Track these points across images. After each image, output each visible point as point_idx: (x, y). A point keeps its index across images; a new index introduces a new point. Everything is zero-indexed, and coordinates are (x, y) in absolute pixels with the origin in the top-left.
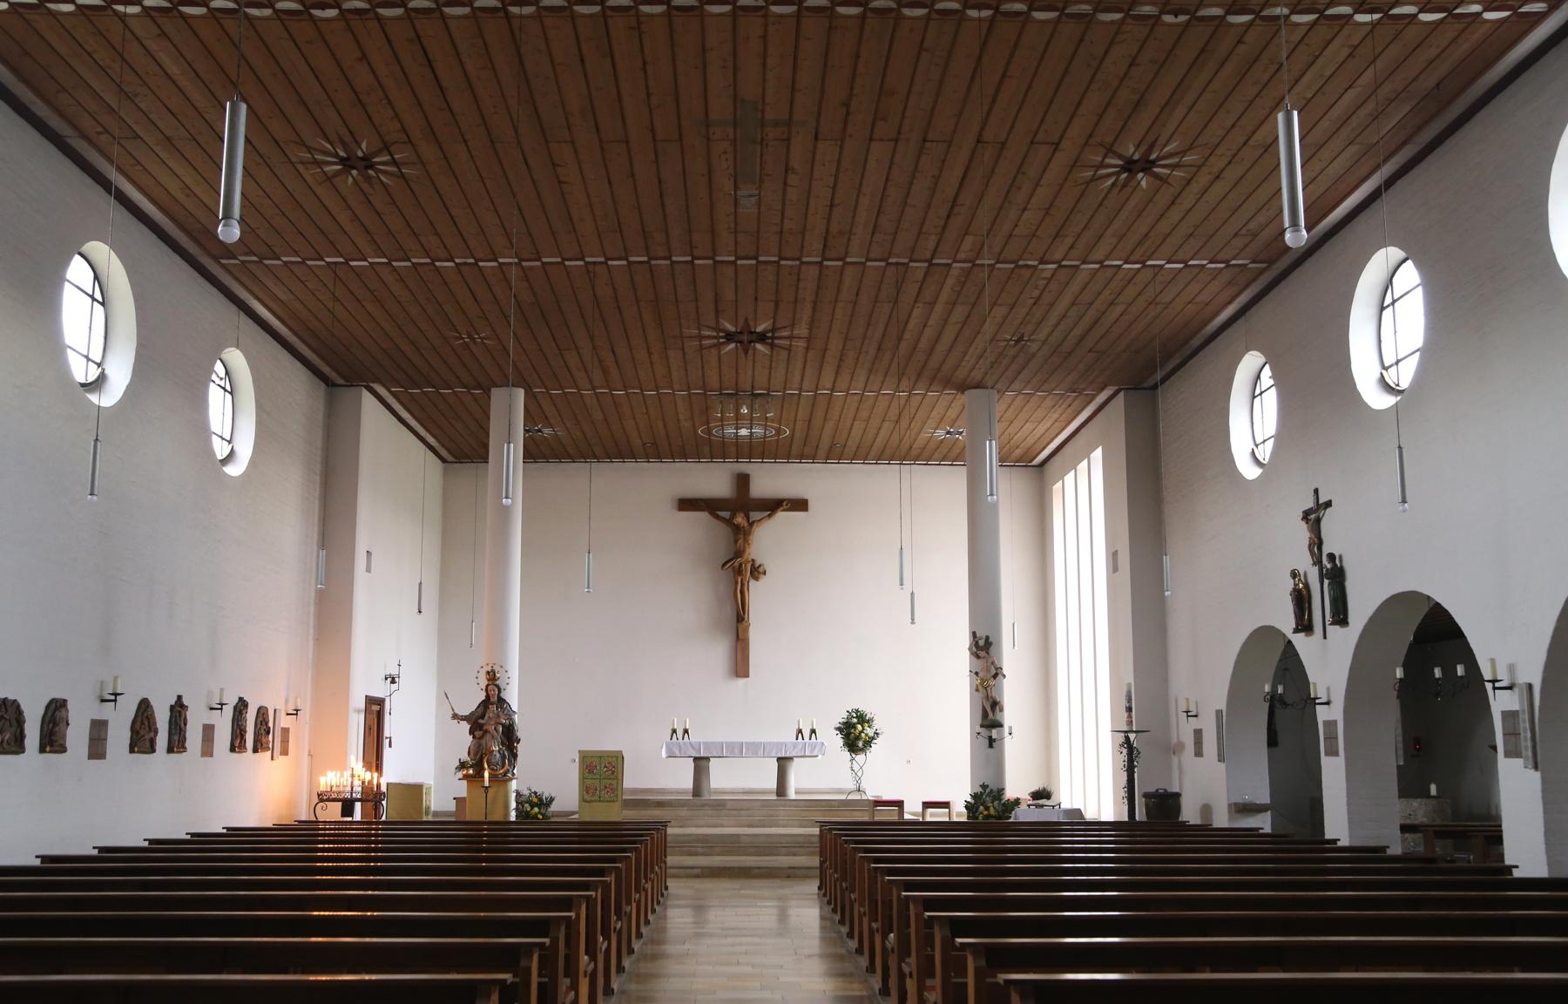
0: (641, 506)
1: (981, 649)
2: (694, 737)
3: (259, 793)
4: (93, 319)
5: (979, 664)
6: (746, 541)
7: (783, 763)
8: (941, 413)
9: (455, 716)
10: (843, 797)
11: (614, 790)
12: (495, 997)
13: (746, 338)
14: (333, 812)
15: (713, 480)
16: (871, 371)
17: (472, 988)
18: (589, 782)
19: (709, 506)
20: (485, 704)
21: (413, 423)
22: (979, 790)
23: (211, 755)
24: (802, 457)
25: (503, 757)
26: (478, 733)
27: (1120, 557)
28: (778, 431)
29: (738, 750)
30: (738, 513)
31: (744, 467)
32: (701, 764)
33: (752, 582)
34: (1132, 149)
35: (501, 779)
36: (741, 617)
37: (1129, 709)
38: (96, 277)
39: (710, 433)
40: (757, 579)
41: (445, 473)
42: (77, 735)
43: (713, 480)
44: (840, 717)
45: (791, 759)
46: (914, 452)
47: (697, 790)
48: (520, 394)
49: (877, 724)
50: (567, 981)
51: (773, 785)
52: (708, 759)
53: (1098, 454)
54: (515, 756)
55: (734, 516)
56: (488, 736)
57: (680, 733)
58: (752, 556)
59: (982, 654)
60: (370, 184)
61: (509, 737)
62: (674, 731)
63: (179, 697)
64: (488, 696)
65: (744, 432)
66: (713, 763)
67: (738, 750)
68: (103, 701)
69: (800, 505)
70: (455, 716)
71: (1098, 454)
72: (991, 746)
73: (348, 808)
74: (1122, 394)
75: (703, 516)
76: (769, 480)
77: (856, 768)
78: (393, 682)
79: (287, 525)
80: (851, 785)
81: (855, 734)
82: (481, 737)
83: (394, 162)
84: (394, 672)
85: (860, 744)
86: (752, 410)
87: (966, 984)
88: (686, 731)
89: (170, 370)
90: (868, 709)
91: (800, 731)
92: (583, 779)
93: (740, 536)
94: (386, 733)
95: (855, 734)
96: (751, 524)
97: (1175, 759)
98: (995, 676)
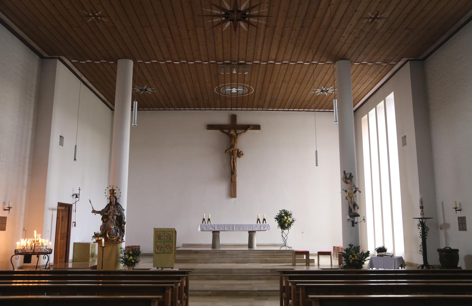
0: (192, 129)
1: (349, 179)
2: (213, 222)
5: (347, 187)
6: (235, 141)
7: (251, 234)
8: (323, 77)
9: (94, 211)
10: (278, 248)
11: (171, 248)
12: (157, 303)
13: (236, 16)
14: (19, 261)
15: (222, 117)
16: (295, 45)
17: (149, 300)
18: (158, 244)
20: (108, 206)
21: (79, 74)
22: (349, 247)
24: (258, 107)
25: (117, 231)
26: (105, 220)
27: (408, 139)
28: (249, 90)
29: (231, 228)
30: (230, 135)
32: (216, 234)
33: (238, 159)
34: (370, 15)
35: (119, 241)
36: (233, 172)
37: (422, 207)
39: (219, 91)
40: (239, 157)
43: (222, 117)
44: (277, 213)
45: (255, 232)
46: (305, 104)
47: (214, 245)
48: (131, 63)
49: (293, 216)
50: (179, 301)
51: (247, 242)
52: (219, 232)
53: (391, 97)
54: (123, 231)
56: (109, 221)
57: (206, 220)
58: (237, 148)
59: (349, 181)
60: (99, 22)
61: (120, 221)
62: (204, 220)
64: (111, 202)
65: (234, 90)
66: (221, 233)
67: (231, 228)
68: (5, 210)
69: (257, 127)
70: (94, 211)
71: (391, 97)
72: (353, 226)
74: (408, 63)
75: (218, 132)
76: (244, 117)
77: (284, 235)
78: (77, 197)
80: (282, 242)
81: (284, 221)
82: (106, 222)
83: (152, 90)
84: (77, 193)
85: (286, 225)
86: (237, 72)
87: (299, 293)
88: (209, 220)
90: (288, 209)
91: (259, 220)
92: (155, 242)
93: (232, 139)
94: (73, 220)
95: (284, 221)
96: (237, 135)
97: (442, 232)
98: (355, 192)
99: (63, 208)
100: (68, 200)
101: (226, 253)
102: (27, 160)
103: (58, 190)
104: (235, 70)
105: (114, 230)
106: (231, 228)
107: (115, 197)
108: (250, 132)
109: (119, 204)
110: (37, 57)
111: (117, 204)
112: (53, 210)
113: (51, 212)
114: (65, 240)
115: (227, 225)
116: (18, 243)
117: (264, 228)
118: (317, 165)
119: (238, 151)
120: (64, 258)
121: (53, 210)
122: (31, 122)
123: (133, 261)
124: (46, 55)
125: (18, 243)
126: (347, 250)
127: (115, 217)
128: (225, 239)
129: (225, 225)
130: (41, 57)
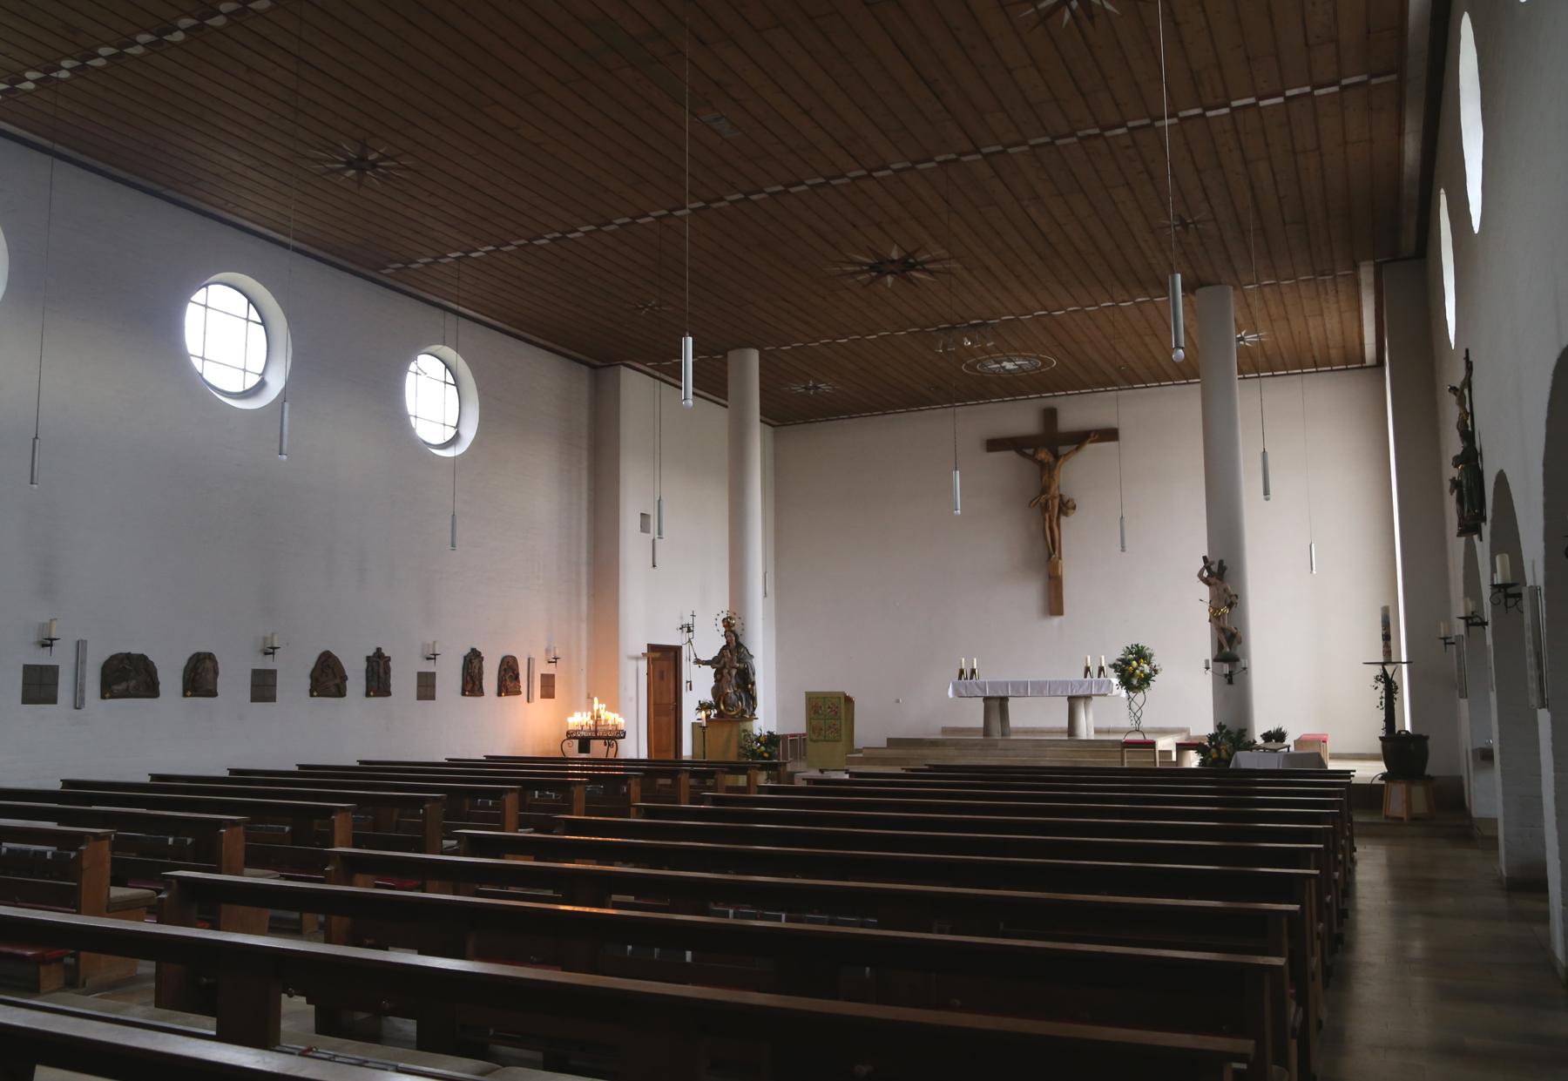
2: (984, 677)
3: (526, 727)
4: (228, 336)
6: (1051, 477)
10: (1121, 737)
14: (573, 750)
15: (1020, 418)
18: (814, 722)
29: (1042, 689)
30: (1047, 448)
31: (1049, 401)
38: (250, 301)
40: (1066, 514)
42: (403, 679)
43: (1020, 418)
44: (1117, 654)
48: (754, 355)
51: (1065, 724)
61: (745, 681)
63: (379, 650)
66: (1013, 705)
69: (1110, 435)
73: (584, 744)
75: (1010, 455)
76: (1077, 412)
79: (540, 497)
85: (1135, 682)
87: (54, 670)
89: (340, 369)
91: (1087, 669)
93: (1047, 471)
96: (1057, 457)
99: (657, 655)
100: (671, 638)
102: (584, 569)
103: (645, 618)
106: (1022, 691)
111: (739, 645)
112: (637, 658)
113: (634, 662)
114: (672, 718)
115: (1014, 684)
116: (570, 720)
118: (1123, 550)
121: (637, 658)
122: (585, 496)
125: (570, 720)
126: (1212, 738)
127: (734, 672)
129: (1007, 684)
130: (593, 367)
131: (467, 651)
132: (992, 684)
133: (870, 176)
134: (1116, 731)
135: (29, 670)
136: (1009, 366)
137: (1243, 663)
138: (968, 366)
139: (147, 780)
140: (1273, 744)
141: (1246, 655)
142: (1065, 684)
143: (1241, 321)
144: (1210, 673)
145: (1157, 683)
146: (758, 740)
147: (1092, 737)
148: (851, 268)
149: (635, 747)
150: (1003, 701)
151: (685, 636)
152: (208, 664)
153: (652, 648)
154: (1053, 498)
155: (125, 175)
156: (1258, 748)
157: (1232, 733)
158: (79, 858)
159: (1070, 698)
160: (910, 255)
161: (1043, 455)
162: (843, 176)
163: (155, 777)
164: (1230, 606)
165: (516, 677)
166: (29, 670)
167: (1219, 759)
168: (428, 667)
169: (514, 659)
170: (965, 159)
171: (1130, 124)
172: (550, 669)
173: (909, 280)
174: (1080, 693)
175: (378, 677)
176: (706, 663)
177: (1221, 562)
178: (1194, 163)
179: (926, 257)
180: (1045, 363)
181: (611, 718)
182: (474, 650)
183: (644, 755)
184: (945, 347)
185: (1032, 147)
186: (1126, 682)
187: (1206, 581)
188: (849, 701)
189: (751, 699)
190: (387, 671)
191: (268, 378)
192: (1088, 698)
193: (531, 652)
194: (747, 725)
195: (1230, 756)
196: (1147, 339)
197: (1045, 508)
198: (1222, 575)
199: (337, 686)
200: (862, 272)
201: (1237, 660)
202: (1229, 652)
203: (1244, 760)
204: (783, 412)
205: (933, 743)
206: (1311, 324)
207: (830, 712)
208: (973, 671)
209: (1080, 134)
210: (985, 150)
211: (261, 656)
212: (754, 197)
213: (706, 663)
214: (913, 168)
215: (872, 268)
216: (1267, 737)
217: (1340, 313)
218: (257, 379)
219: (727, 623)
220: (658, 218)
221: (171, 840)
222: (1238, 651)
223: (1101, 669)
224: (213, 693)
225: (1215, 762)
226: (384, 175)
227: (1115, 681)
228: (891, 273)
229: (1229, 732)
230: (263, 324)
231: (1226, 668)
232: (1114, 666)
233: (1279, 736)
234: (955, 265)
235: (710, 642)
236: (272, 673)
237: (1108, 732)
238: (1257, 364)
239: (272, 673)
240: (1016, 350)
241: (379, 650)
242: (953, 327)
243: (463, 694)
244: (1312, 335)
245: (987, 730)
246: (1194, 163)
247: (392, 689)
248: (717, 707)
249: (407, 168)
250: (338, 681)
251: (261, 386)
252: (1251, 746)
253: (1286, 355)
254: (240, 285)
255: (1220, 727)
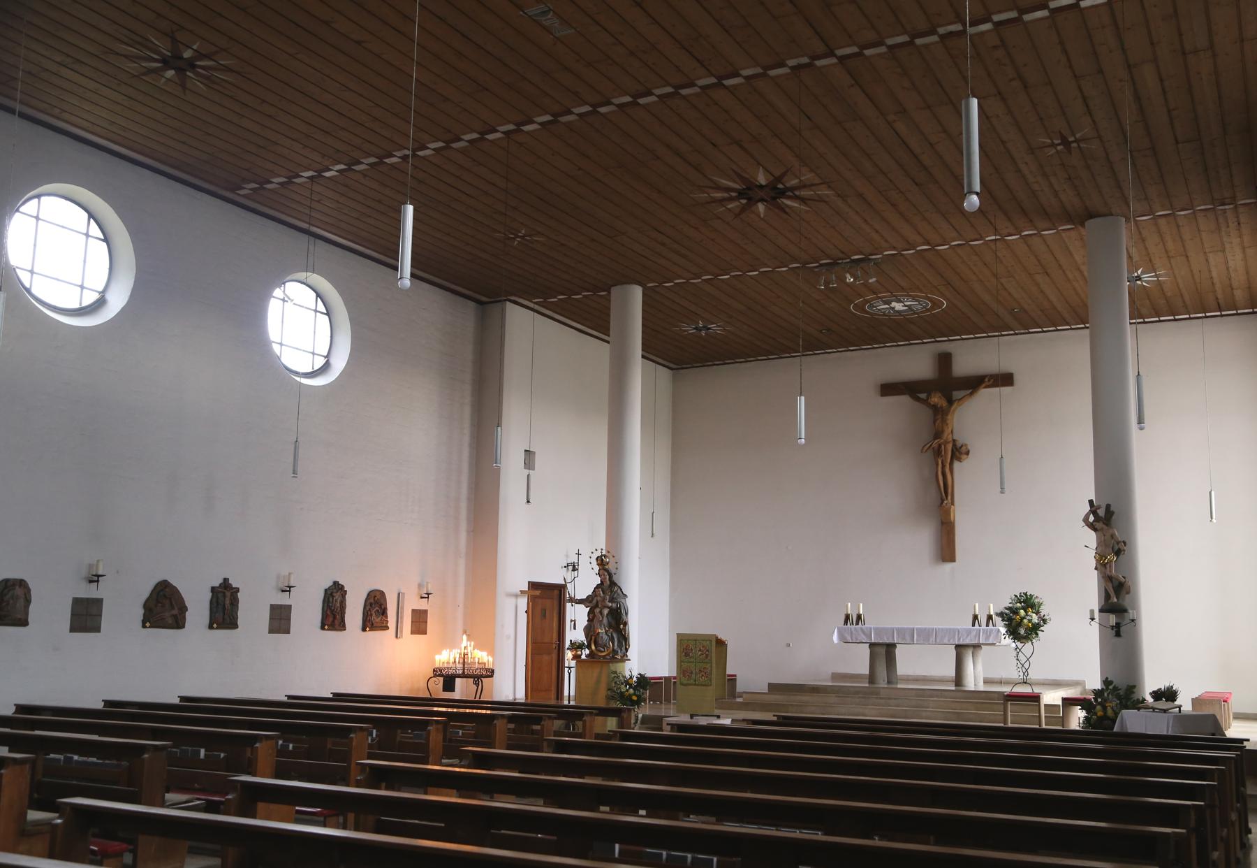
2: (870, 623)
3: (390, 664)
6: (944, 421)
10: (1006, 689)
15: (915, 362)
18: (685, 665)
19: (910, 389)
23: (287, 631)
29: (927, 636)
30: (942, 392)
40: (959, 460)
41: (675, 380)
42: (253, 612)
43: (915, 362)
44: (1005, 602)
48: (637, 293)
49: (1044, 611)
51: (951, 672)
55: (929, 396)
61: (617, 620)
63: (226, 580)
66: (900, 652)
69: (1005, 380)
73: (449, 684)
75: (905, 399)
76: (972, 356)
77: (1023, 659)
78: (574, 570)
79: (417, 428)
85: (1022, 631)
91: (975, 617)
93: (940, 415)
96: (950, 402)
99: (537, 593)
100: (554, 576)
101: (878, 694)
102: (464, 505)
104: (848, 276)
105: (605, 637)
107: (607, 571)
108: (986, 394)
109: (615, 584)
110: (472, 304)
111: (613, 584)
112: (516, 596)
113: (513, 600)
114: (554, 656)
116: (438, 658)
117: (988, 638)
118: (1002, 490)
119: (954, 445)
120: (554, 688)
122: (467, 431)
123: (635, 698)
124: (484, 299)
125: (438, 658)
126: (1097, 693)
127: (606, 611)
128: (910, 663)
131: (329, 584)
132: (879, 631)
133: (719, 85)
134: (1007, 682)
135: (77, 602)
136: (898, 306)
137: (1131, 614)
138: (856, 306)
139: (100, 706)
140: (1163, 704)
141: (1136, 606)
142: (952, 632)
143: (1136, 258)
144: (1096, 625)
145: (1046, 632)
146: (627, 683)
147: (982, 687)
148: (719, 195)
149: (510, 686)
150: (890, 648)
151: (570, 575)
152: (19, 591)
153: (533, 585)
154: (946, 443)
155: (206, 186)
156: (1147, 708)
157: (1118, 693)
158: (542, 729)
159: (958, 647)
160: (779, 179)
161: (936, 399)
162: (692, 85)
163: (108, 703)
164: (1118, 553)
165: (384, 612)
166: (77, 602)
167: (1105, 717)
168: (282, 599)
169: (382, 593)
170: (819, 63)
171: (996, 18)
172: (422, 605)
173: (782, 209)
174: (967, 641)
175: (224, 607)
176: (580, 602)
177: (1108, 506)
178: (1071, 67)
179: (794, 182)
180: (936, 304)
181: (481, 657)
182: (336, 583)
183: (521, 696)
184: (827, 283)
185: (890, 47)
186: (1013, 632)
187: (1092, 526)
188: (721, 644)
189: (624, 639)
190: (235, 602)
191: (109, 296)
192: (976, 647)
193: (403, 590)
194: (618, 667)
195: (1116, 714)
196: (1039, 278)
197: (938, 453)
198: (1109, 521)
199: (175, 617)
200: (731, 199)
201: (1125, 611)
202: (1117, 602)
203: (1132, 721)
204: (675, 349)
205: (815, 690)
206: (1211, 260)
207: (701, 654)
208: (859, 617)
209: (941, 31)
210: (840, 52)
211: (84, 584)
212: (603, 110)
213: (580, 602)
214: (764, 75)
215: (741, 194)
216: (1157, 695)
217: (1244, 249)
218: (95, 296)
219: (601, 561)
220: (507, 133)
221: (291, 746)
222: (1126, 602)
223: (990, 618)
224: (24, 623)
225: (1101, 719)
226: (208, 78)
227: (1003, 630)
228: (762, 200)
229: (1116, 689)
230: (328, 314)
231: (1113, 619)
232: (1001, 615)
233: (1168, 695)
234: (824, 191)
235: (585, 583)
236: (288, 608)
237: (1001, 682)
238: (1154, 307)
239: (288, 608)
240: (903, 289)
241: (226, 580)
242: (834, 264)
243: (323, 628)
244: (1214, 274)
245: (872, 678)
246: (1071, 67)
247: (239, 622)
248: (589, 647)
249: (228, 69)
250: (175, 612)
251: (100, 303)
252: (1139, 704)
253: (1187, 297)
254: (76, 198)
255: (1106, 682)
